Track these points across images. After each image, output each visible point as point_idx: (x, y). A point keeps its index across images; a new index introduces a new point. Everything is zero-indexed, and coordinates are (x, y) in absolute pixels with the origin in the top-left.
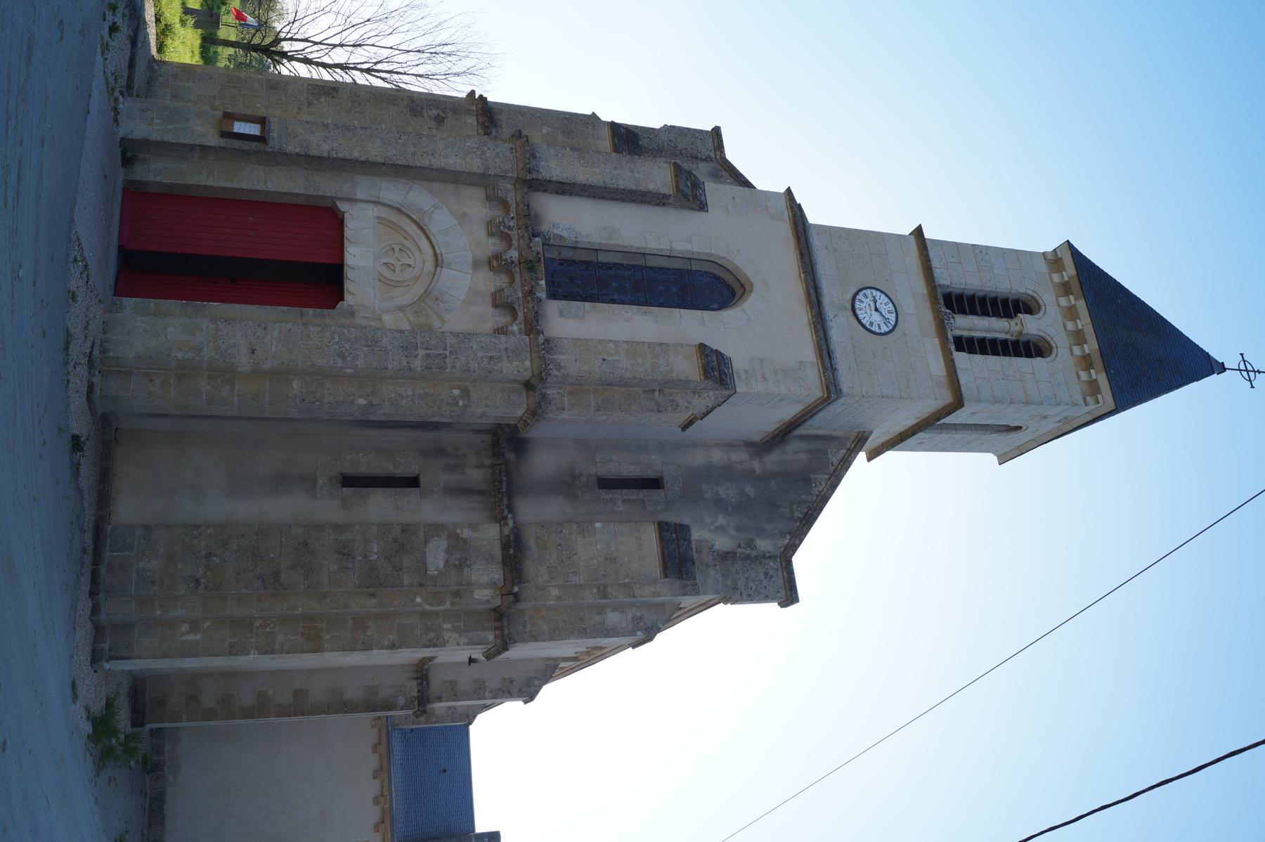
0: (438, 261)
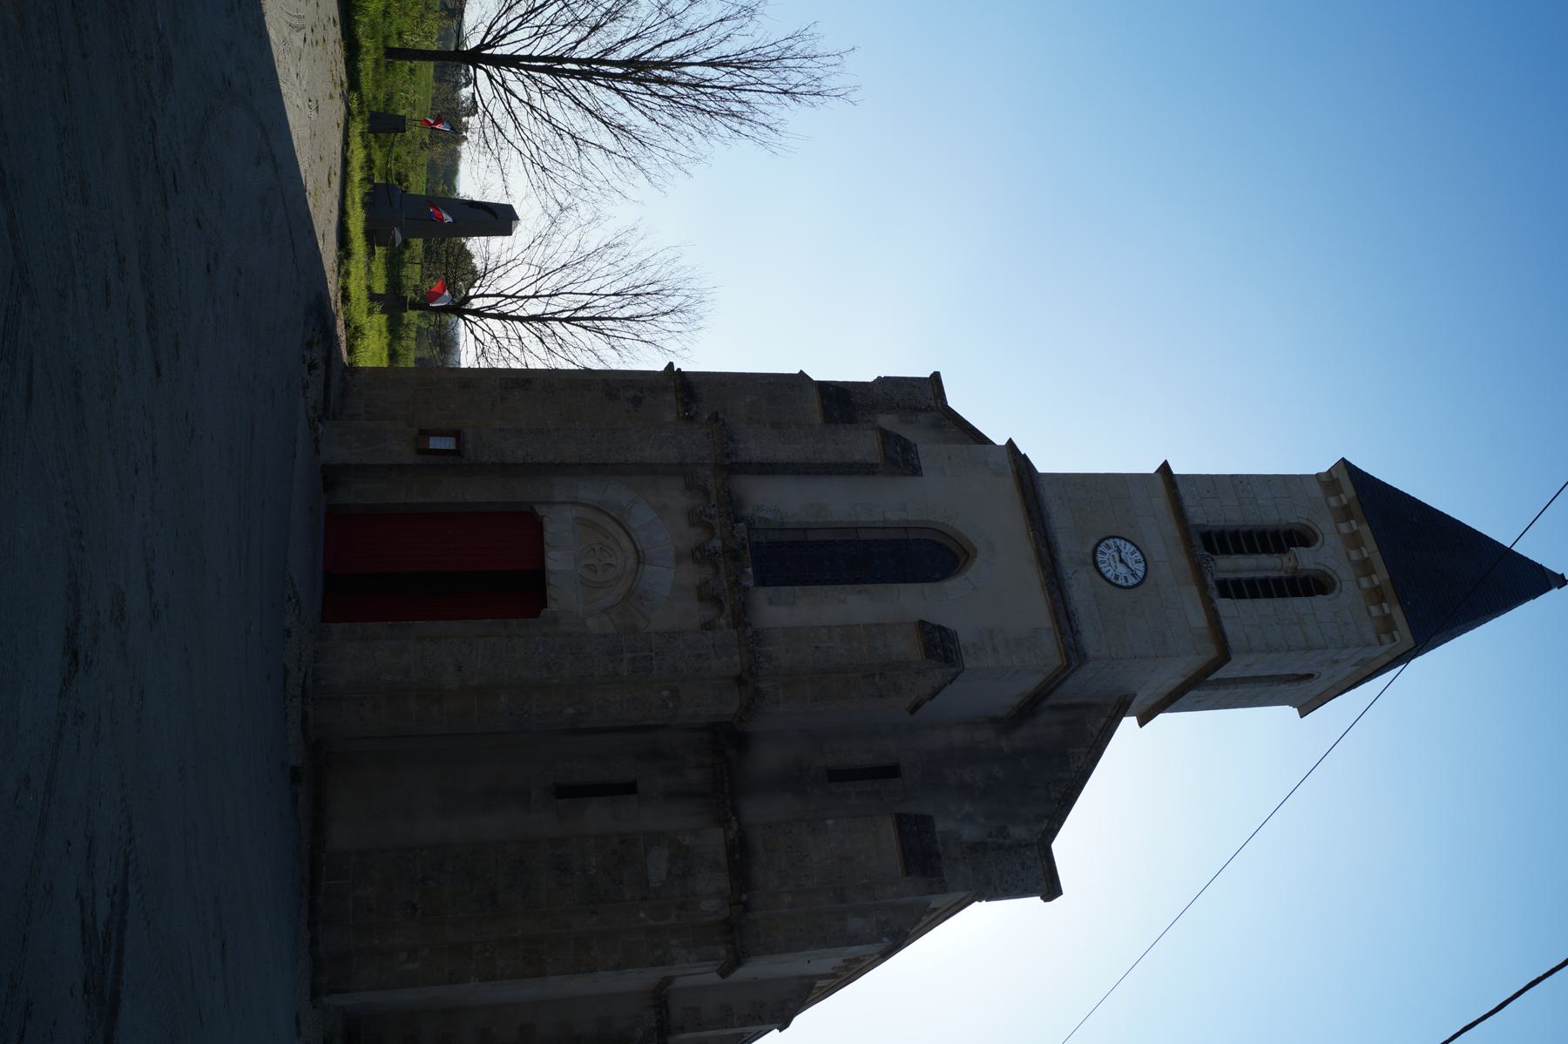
0: (640, 559)
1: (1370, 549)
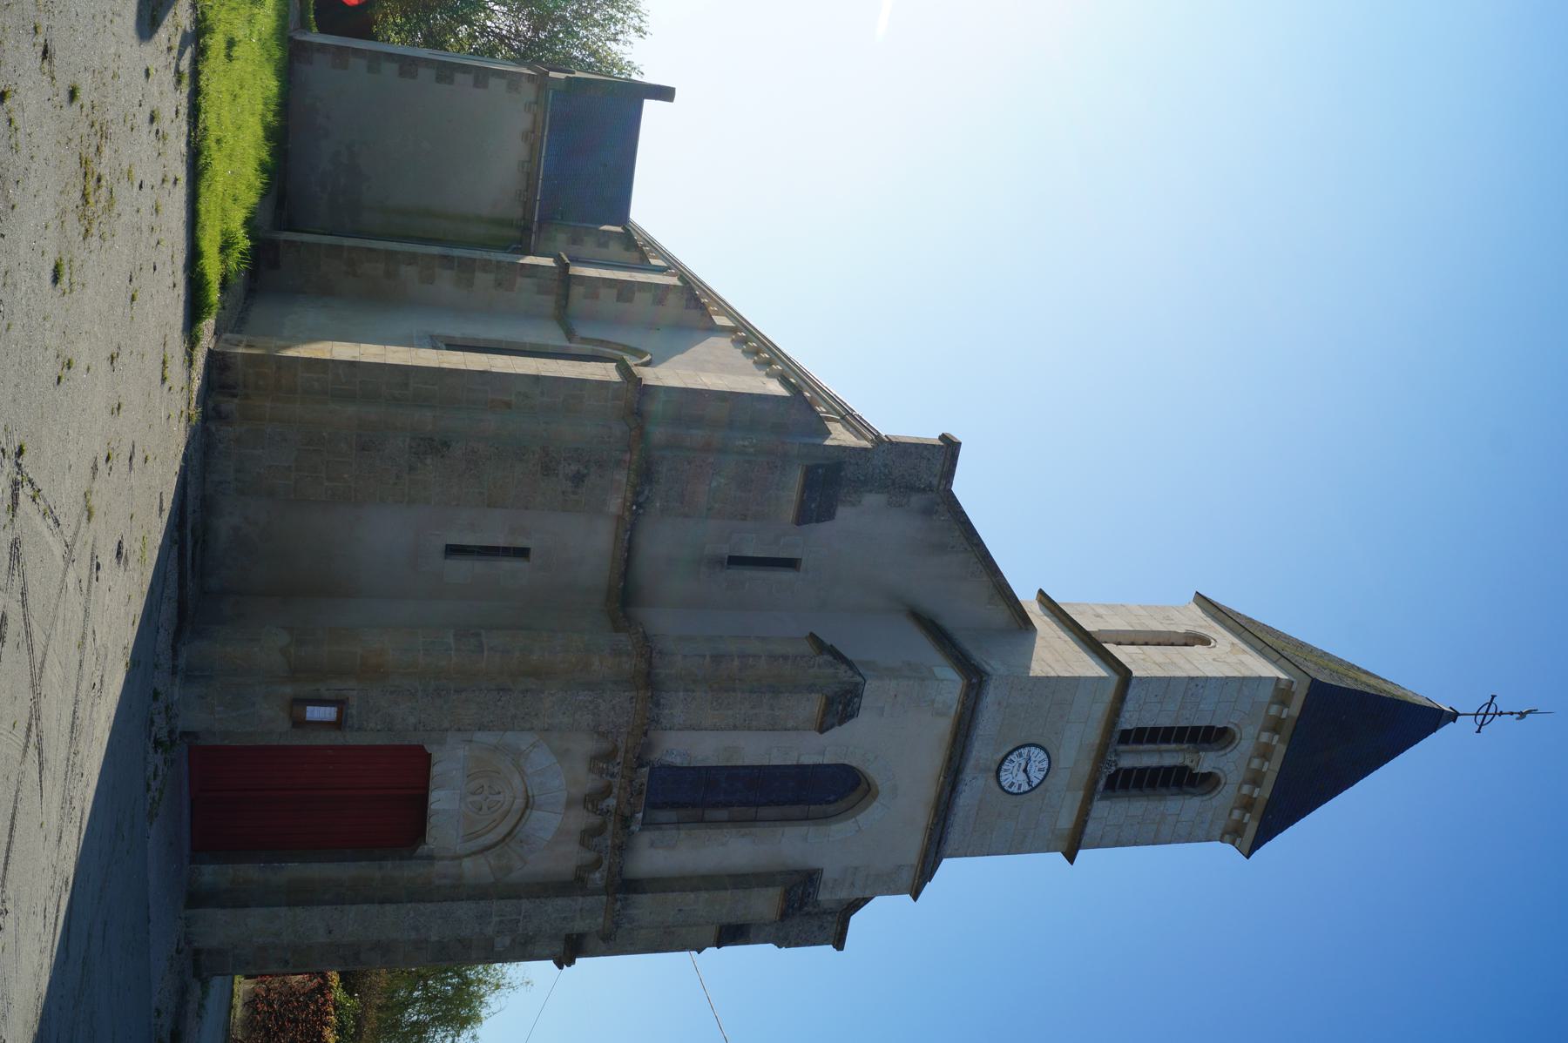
1: (1272, 768)
